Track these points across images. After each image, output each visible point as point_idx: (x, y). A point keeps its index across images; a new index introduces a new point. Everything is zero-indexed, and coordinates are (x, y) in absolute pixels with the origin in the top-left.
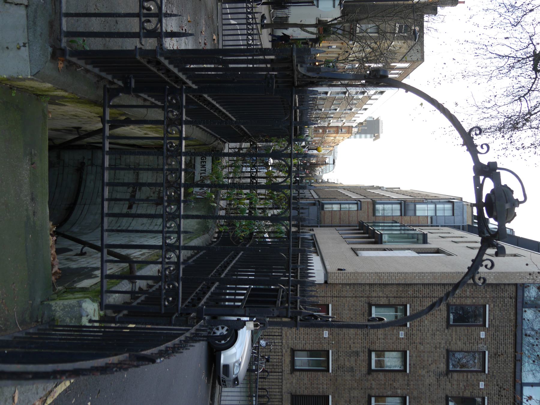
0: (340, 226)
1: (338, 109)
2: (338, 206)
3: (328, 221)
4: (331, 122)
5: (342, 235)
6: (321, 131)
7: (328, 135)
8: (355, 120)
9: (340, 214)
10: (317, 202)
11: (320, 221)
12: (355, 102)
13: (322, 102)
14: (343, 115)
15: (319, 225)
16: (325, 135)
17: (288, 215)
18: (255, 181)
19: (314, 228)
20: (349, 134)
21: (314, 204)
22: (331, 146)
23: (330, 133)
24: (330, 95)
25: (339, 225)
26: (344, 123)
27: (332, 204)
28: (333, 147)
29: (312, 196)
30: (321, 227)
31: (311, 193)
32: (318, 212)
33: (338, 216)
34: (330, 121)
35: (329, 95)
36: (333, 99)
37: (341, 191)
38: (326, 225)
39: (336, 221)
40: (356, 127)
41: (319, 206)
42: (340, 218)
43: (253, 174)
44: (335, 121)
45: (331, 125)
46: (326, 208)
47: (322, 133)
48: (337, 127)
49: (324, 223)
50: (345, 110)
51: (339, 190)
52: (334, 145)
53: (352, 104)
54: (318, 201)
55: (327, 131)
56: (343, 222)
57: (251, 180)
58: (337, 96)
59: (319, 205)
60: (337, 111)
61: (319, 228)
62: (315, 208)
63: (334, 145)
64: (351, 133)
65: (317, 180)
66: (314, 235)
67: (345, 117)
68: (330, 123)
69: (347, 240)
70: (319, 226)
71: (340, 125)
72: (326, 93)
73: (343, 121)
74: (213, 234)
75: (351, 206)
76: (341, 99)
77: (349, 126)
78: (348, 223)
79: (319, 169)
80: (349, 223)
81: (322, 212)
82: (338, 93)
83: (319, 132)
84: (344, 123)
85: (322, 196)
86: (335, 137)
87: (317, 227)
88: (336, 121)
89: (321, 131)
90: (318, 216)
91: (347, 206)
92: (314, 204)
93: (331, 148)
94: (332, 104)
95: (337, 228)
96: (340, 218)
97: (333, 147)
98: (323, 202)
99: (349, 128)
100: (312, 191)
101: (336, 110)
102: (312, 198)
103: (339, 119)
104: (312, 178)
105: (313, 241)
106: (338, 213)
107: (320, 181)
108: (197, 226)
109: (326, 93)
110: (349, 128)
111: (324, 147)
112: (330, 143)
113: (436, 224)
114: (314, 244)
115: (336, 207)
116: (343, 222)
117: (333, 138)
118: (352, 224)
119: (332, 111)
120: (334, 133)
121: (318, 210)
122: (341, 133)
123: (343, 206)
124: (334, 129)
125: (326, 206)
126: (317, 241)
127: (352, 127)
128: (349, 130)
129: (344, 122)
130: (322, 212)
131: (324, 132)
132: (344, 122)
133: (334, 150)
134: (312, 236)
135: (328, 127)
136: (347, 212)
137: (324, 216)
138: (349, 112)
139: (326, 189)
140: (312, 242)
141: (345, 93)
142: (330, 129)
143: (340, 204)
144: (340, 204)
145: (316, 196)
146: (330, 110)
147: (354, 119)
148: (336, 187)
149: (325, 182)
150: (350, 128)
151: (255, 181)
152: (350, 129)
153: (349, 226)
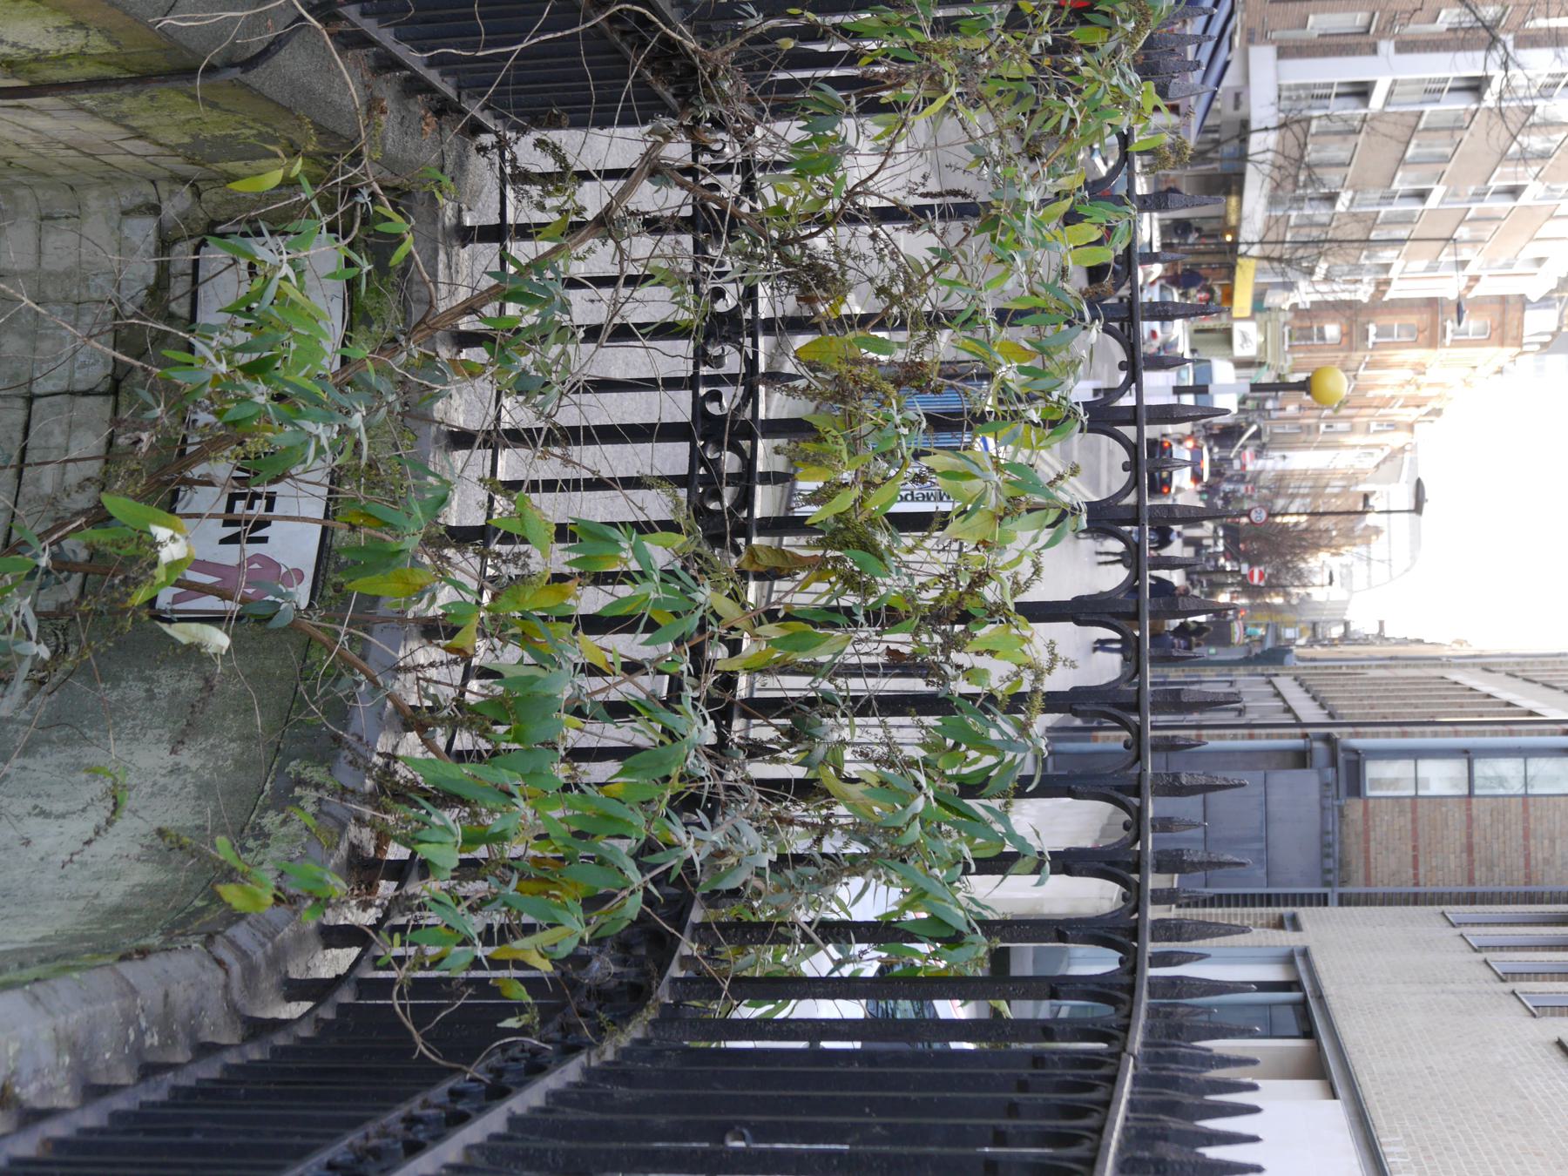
0: (1471, 899)
1: (1438, 191)
2: (1456, 768)
3: (1389, 866)
4: (1393, 274)
5: (1490, 956)
6: (1332, 331)
7: (1377, 355)
8: (1540, 261)
9: (1470, 819)
10: (1318, 745)
11: (1343, 864)
12: (1535, 142)
13: (1336, 150)
14: (1463, 232)
15: (1333, 893)
16: (1357, 356)
17: (52, 241)
18: (731, 462)
19: (1303, 913)
20: (1502, 343)
21: (1301, 759)
22: (1394, 426)
23: (1387, 346)
24: (1387, 102)
25: (1466, 889)
26: (1476, 279)
27: (1416, 754)
28: (1411, 428)
29: (1289, 710)
30: (1344, 901)
31: (1278, 695)
32: (1323, 808)
33: (1456, 837)
34: (1387, 267)
35: (1377, 101)
36: (1400, 132)
37: (1470, 683)
38: (1380, 889)
39: (1446, 870)
40: (1546, 301)
41: (1330, 772)
42: (1470, 848)
43: (716, 397)
44: (1419, 265)
45: (1391, 294)
46: (1378, 783)
47: (1338, 346)
48: (1432, 304)
49: (1367, 880)
50: (1479, 196)
51: (1455, 675)
52: (1411, 414)
53: (1524, 157)
54: (1328, 739)
55: (1372, 329)
56: (1490, 869)
57: (696, 458)
58: (1428, 109)
59: (1333, 762)
60: (1433, 202)
61: (1333, 911)
62: (1306, 785)
63: (1411, 414)
64: (1518, 341)
65: (1314, 625)
66: (1305, 953)
67: (1475, 241)
68: (1388, 282)
69: (1520, 986)
70: (1333, 898)
71: (1449, 287)
72: (1362, 91)
73: (1463, 264)
74: (277, 959)
75: (1538, 766)
76: (1452, 129)
77: (1503, 300)
78: (1519, 875)
79: (1318, 563)
80: (1528, 878)
81: (1355, 808)
82: (1433, 91)
83: (1322, 337)
84: (1476, 279)
85: (1347, 711)
86: (1420, 369)
87: (1323, 900)
88: (1424, 263)
89: (1332, 331)
90: (1324, 832)
91: (1509, 768)
92: (1301, 759)
93: (1397, 439)
94: (1401, 161)
95: (1453, 910)
96: (1470, 848)
97: (1411, 428)
98: (1356, 743)
99: (1504, 313)
100: (1285, 684)
101: (1422, 195)
102: (1287, 718)
103: (1447, 257)
104: (1288, 617)
105: (1295, 996)
106: (1457, 815)
107: (1336, 632)
108: (143, 874)
109: (1362, 91)
110: (1504, 313)
111: (1352, 430)
112: (1387, 403)
113: (1364, 890)
114: (1302, 1008)
115: (1441, 778)
116: (1490, 869)
117: (1407, 374)
118: (1549, 885)
119: (1400, 207)
120: (1415, 344)
121: (1323, 797)
122: (1456, 344)
123: (1483, 768)
124: (1413, 319)
125: (1374, 770)
126: (1320, 997)
127: (1523, 302)
128: (1502, 324)
129: (1471, 270)
130: (1355, 808)
131: (1353, 338)
132: (1471, 270)
133: (1415, 448)
134: (1289, 960)
135: (1378, 306)
136: (1516, 807)
137: (1366, 832)
138: (1503, 205)
139: (1373, 673)
140: (1294, 1004)
141: (1476, 87)
142: (1385, 320)
143: (1468, 754)
144: (1468, 754)
145: (1309, 711)
146: (1388, 198)
147: (1535, 250)
148: (1436, 661)
149: (1366, 641)
150: (1509, 309)
151: (731, 462)
152: (1512, 315)
153: (1530, 899)
